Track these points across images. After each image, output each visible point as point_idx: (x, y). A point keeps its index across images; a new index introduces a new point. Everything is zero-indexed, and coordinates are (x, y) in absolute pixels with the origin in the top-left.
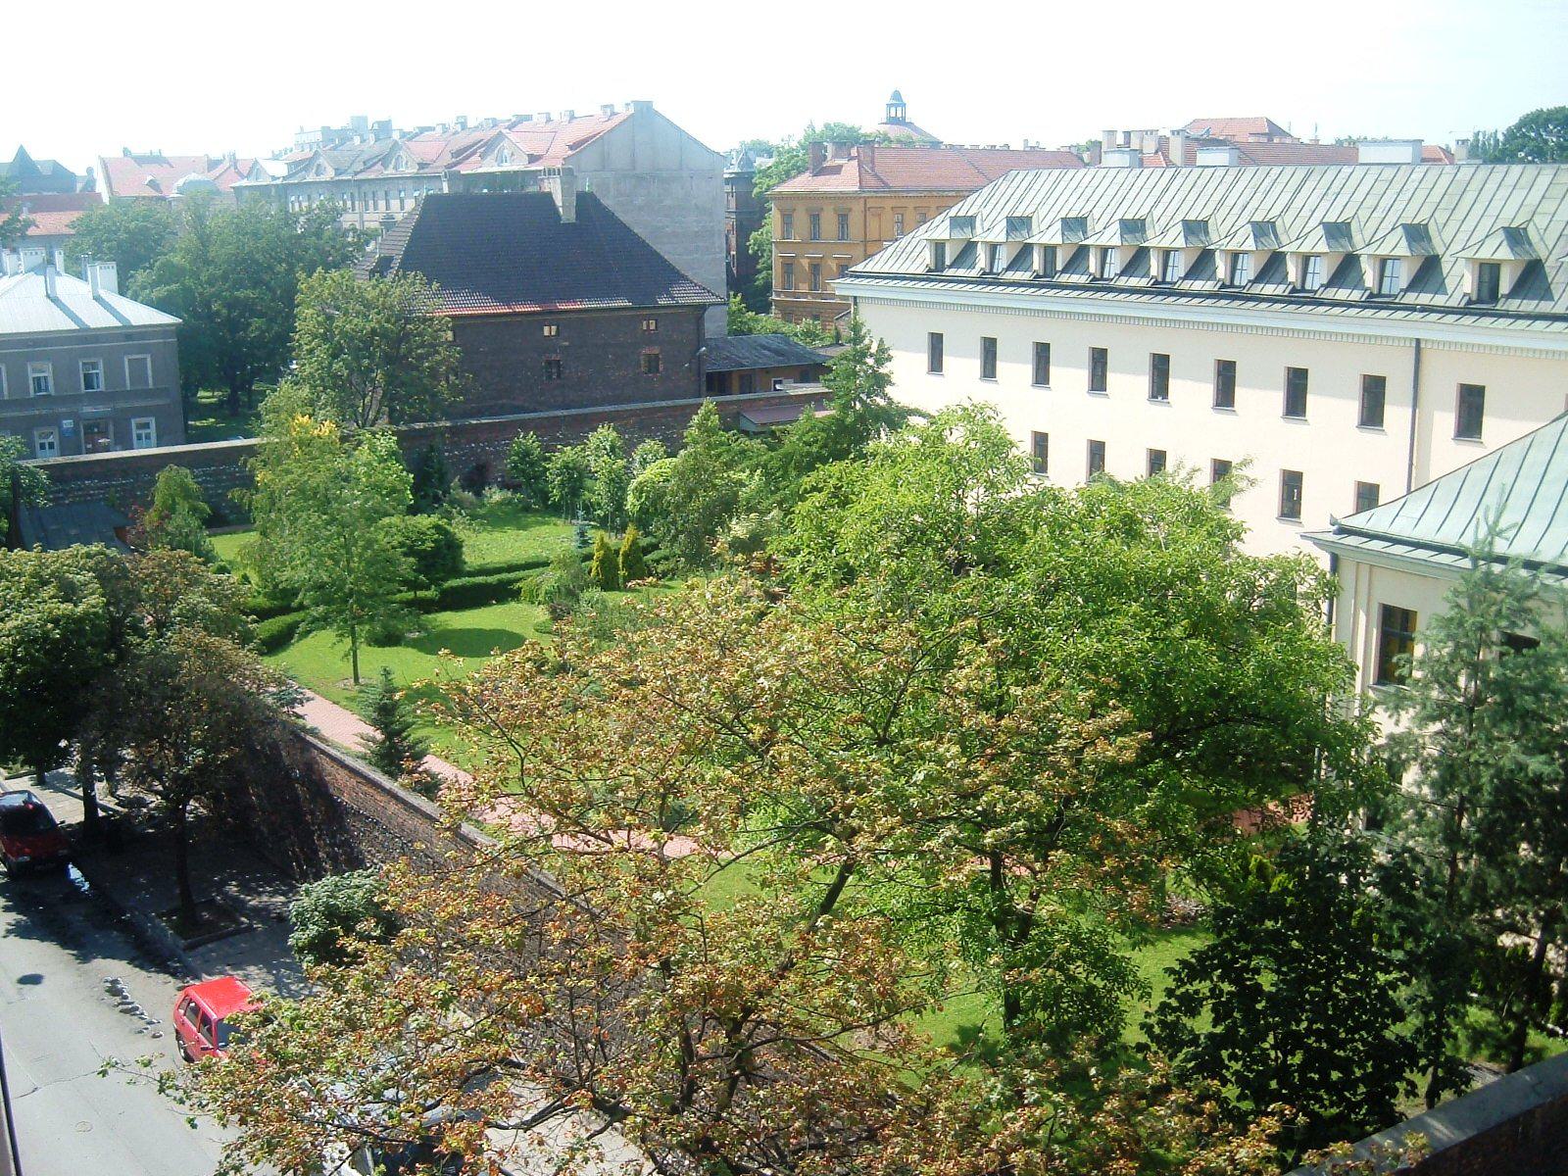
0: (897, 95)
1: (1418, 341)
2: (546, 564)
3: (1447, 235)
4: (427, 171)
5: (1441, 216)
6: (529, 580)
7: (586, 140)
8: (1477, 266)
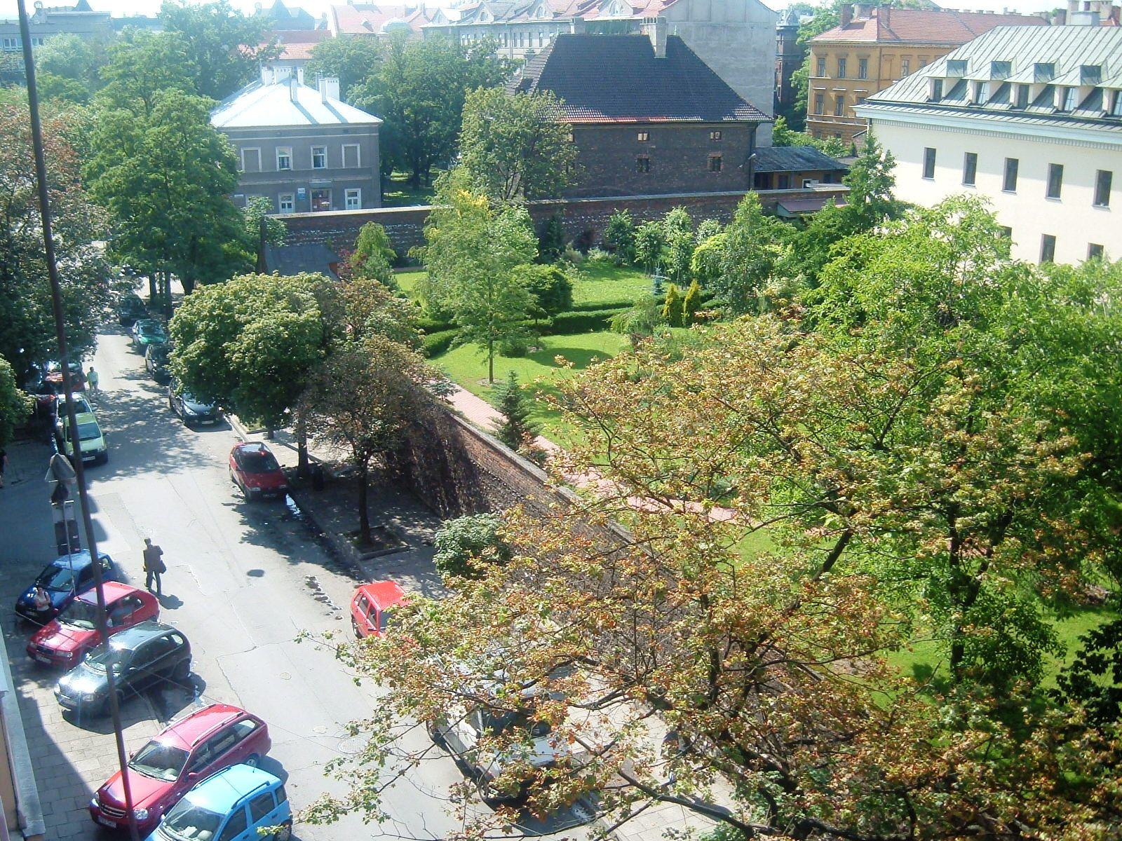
2: (630, 305)
6: (617, 316)
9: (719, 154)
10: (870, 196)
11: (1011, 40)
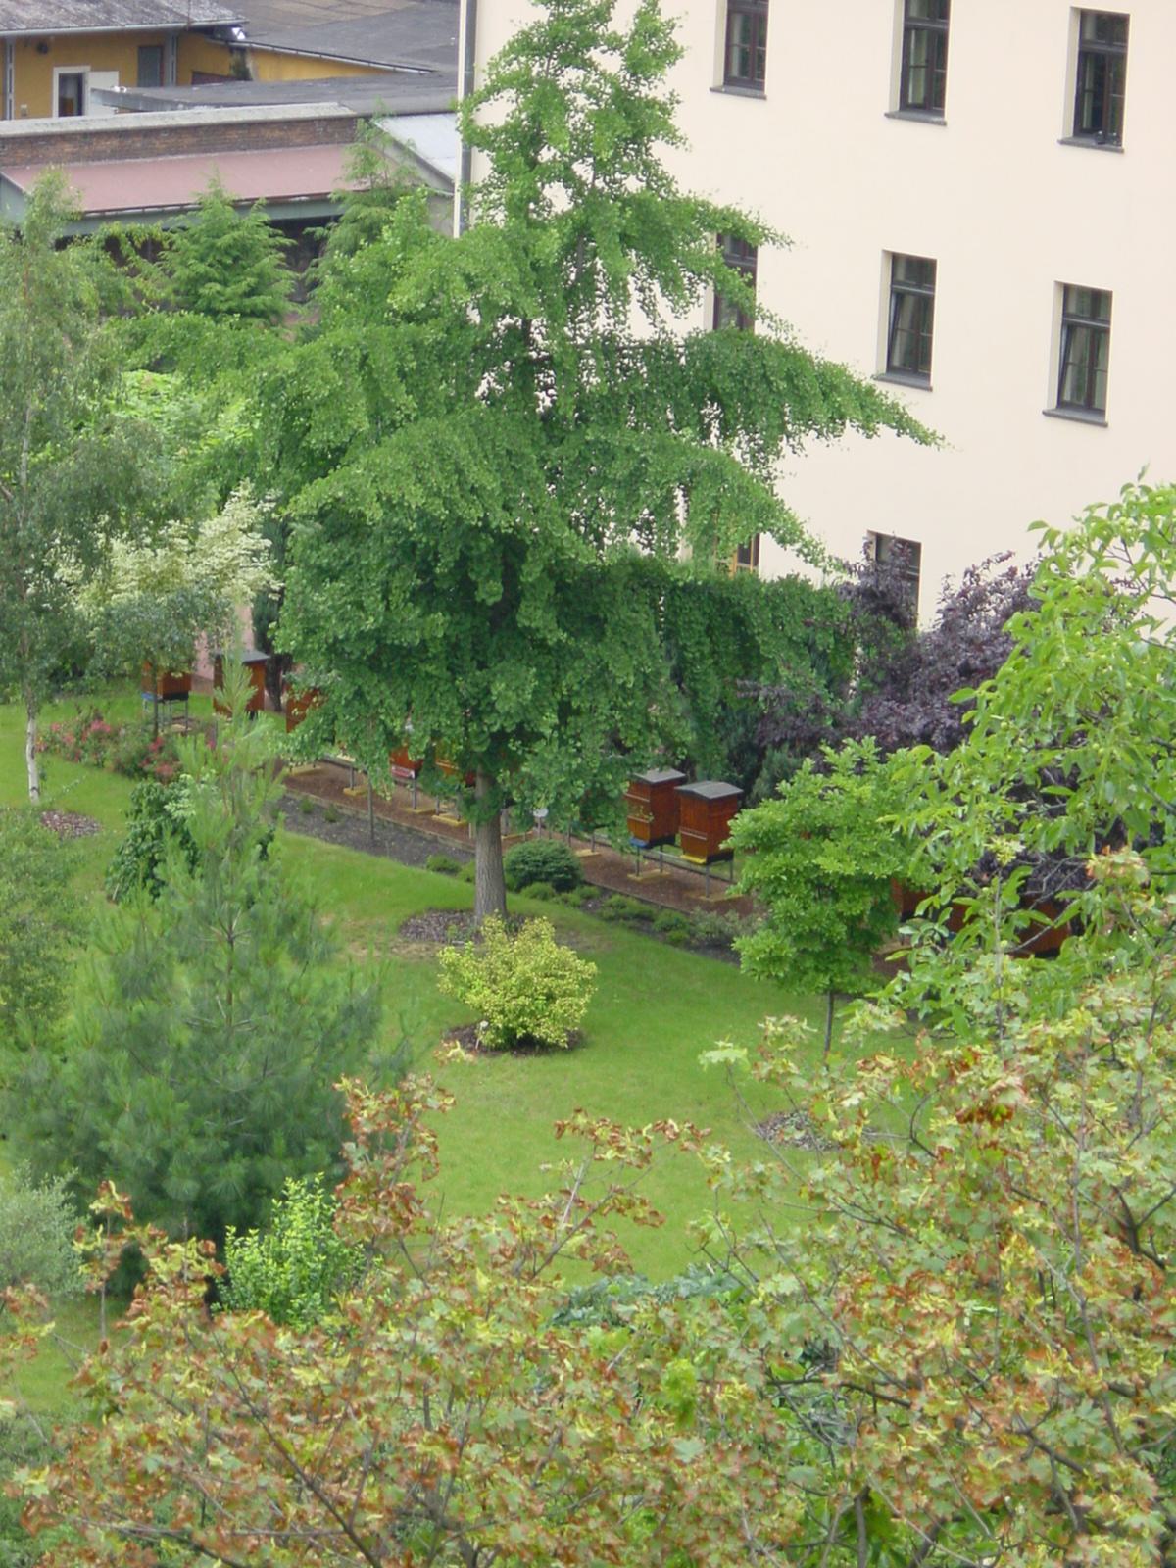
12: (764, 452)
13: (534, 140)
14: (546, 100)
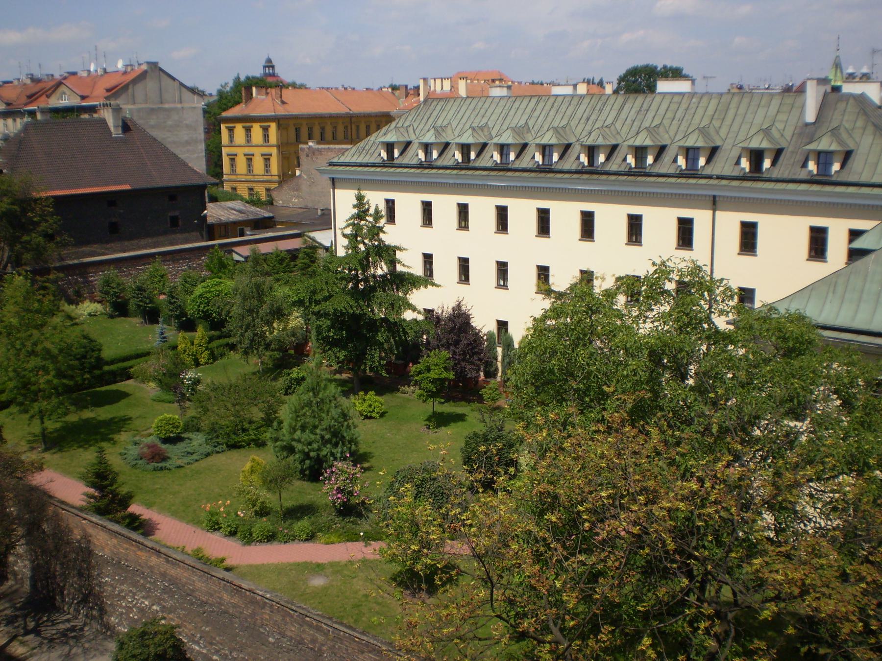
0: (269, 61)
1: (714, 197)
2: (148, 354)
3: (723, 132)
4: (11, 109)
5: (716, 123)
6: (137, 366)
7: (37, 93)
8: (587, 149)
9: (177, 213)
10: (364, 244)
11: (534, 110)
12: (406, 293)
13: (356, 236)
14: (357, 228)
